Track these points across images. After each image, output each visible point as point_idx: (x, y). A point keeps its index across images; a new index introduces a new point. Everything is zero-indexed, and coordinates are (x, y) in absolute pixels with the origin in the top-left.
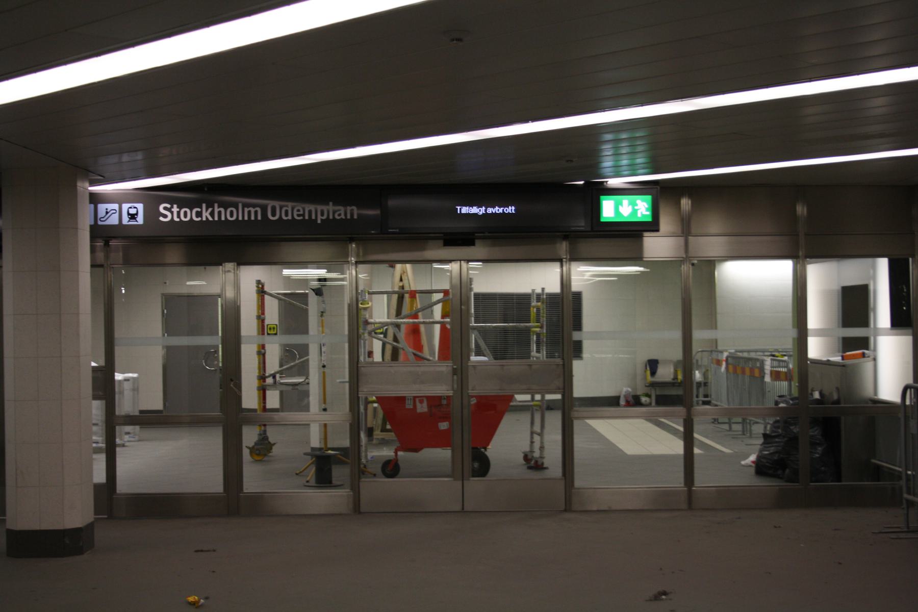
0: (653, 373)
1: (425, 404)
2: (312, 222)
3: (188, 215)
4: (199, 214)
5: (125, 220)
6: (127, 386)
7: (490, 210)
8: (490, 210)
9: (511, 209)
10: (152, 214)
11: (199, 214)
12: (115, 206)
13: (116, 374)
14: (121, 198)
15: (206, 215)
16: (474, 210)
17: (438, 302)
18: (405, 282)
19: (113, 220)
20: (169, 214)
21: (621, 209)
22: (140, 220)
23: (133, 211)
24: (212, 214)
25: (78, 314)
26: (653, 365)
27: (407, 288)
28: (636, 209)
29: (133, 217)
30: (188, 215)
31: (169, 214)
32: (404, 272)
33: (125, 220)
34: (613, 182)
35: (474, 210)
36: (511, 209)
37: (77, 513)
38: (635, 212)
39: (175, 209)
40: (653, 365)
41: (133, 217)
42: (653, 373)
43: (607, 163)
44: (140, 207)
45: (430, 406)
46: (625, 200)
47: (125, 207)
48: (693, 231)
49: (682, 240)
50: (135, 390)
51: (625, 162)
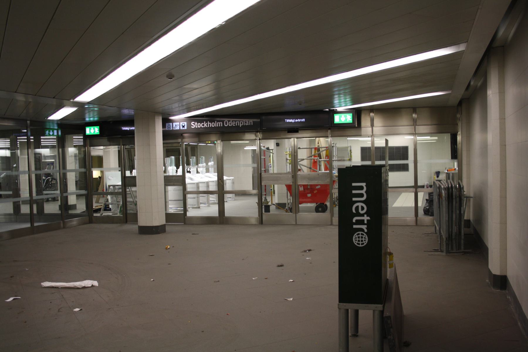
0: (438, 177)
1: (302, 188)
2: (238, 126)
3: (200, 125)
4: (203, 125)
5: (181, 128)
6: (227, 181)
7: (296, 121)
8: (296, 121)
9: (303, 120)
10: (189, 125)
11: (203, 125)
12: (178, 123)
13: (224, 177)
14: (180, 121)
15: (205, 125)
16: (291, 121)
17: (324, 151)
18: (320, 144)
19: (178, 128)
20: (195, 125)
21: (341, 119)
22: (186, 128)
23: (183, 125)
24: (207, 125)
25: (156, 159)
26: (438, 174)
27: (320, 146)
28: (348, 118)
29: (183, 127)
30: (200, 125)
31: (195, 125)
32: (319, 140)
33: (181, 128)
34: (339, 109)
35: (291, 121)
36: (303, 120)
37: (159, 220)
38: (346, 119)
39: (196, 124)
40: (438, 174)
41: (183, 127)
42: (438, 177)
43: (336, 101)
44: (186, 123)
45: (304, 189)
46: (343, 115)
47: (181, 123)
48: (418, 124)
49: (413, 127)
50: (233, 183)
51: (342, 101)
